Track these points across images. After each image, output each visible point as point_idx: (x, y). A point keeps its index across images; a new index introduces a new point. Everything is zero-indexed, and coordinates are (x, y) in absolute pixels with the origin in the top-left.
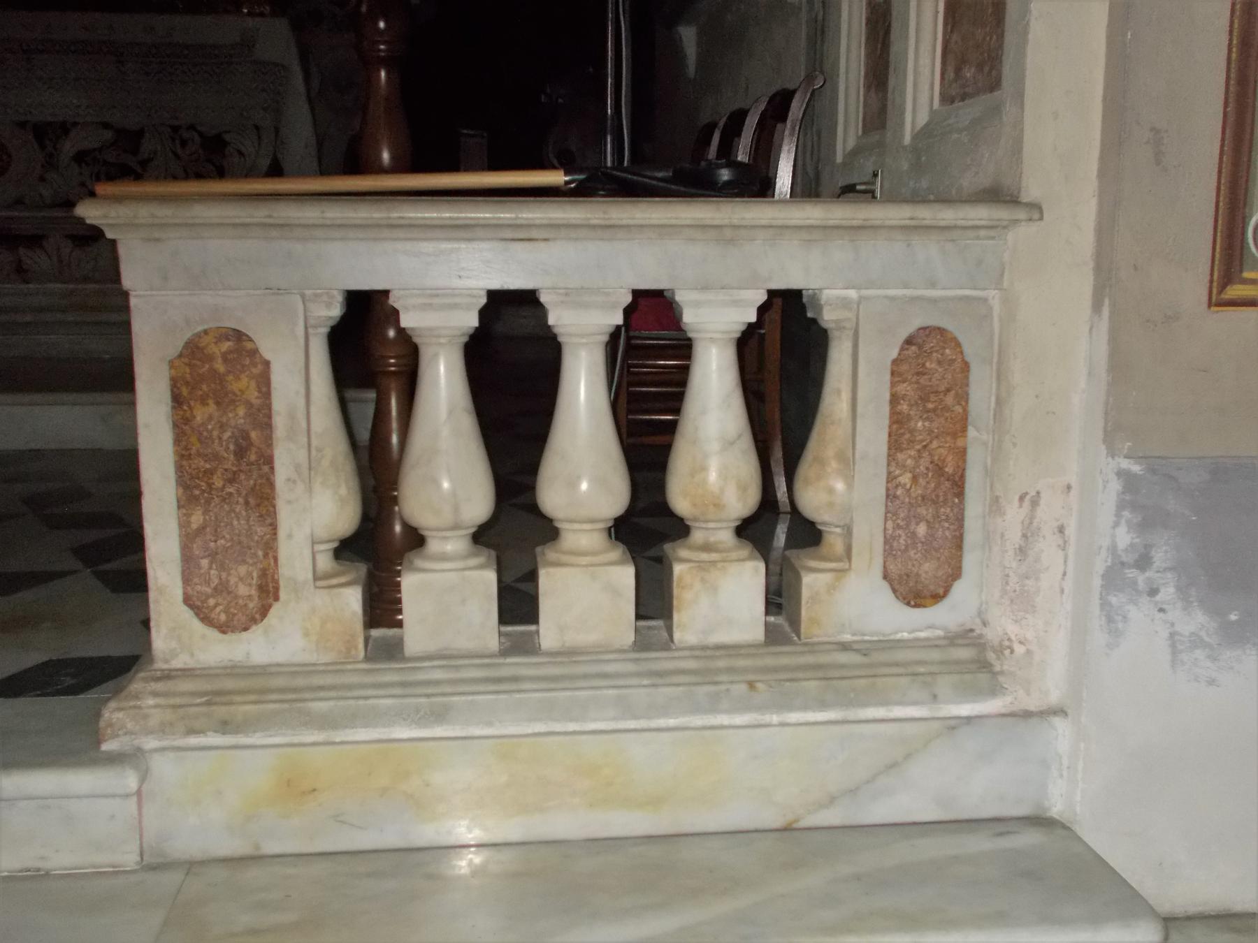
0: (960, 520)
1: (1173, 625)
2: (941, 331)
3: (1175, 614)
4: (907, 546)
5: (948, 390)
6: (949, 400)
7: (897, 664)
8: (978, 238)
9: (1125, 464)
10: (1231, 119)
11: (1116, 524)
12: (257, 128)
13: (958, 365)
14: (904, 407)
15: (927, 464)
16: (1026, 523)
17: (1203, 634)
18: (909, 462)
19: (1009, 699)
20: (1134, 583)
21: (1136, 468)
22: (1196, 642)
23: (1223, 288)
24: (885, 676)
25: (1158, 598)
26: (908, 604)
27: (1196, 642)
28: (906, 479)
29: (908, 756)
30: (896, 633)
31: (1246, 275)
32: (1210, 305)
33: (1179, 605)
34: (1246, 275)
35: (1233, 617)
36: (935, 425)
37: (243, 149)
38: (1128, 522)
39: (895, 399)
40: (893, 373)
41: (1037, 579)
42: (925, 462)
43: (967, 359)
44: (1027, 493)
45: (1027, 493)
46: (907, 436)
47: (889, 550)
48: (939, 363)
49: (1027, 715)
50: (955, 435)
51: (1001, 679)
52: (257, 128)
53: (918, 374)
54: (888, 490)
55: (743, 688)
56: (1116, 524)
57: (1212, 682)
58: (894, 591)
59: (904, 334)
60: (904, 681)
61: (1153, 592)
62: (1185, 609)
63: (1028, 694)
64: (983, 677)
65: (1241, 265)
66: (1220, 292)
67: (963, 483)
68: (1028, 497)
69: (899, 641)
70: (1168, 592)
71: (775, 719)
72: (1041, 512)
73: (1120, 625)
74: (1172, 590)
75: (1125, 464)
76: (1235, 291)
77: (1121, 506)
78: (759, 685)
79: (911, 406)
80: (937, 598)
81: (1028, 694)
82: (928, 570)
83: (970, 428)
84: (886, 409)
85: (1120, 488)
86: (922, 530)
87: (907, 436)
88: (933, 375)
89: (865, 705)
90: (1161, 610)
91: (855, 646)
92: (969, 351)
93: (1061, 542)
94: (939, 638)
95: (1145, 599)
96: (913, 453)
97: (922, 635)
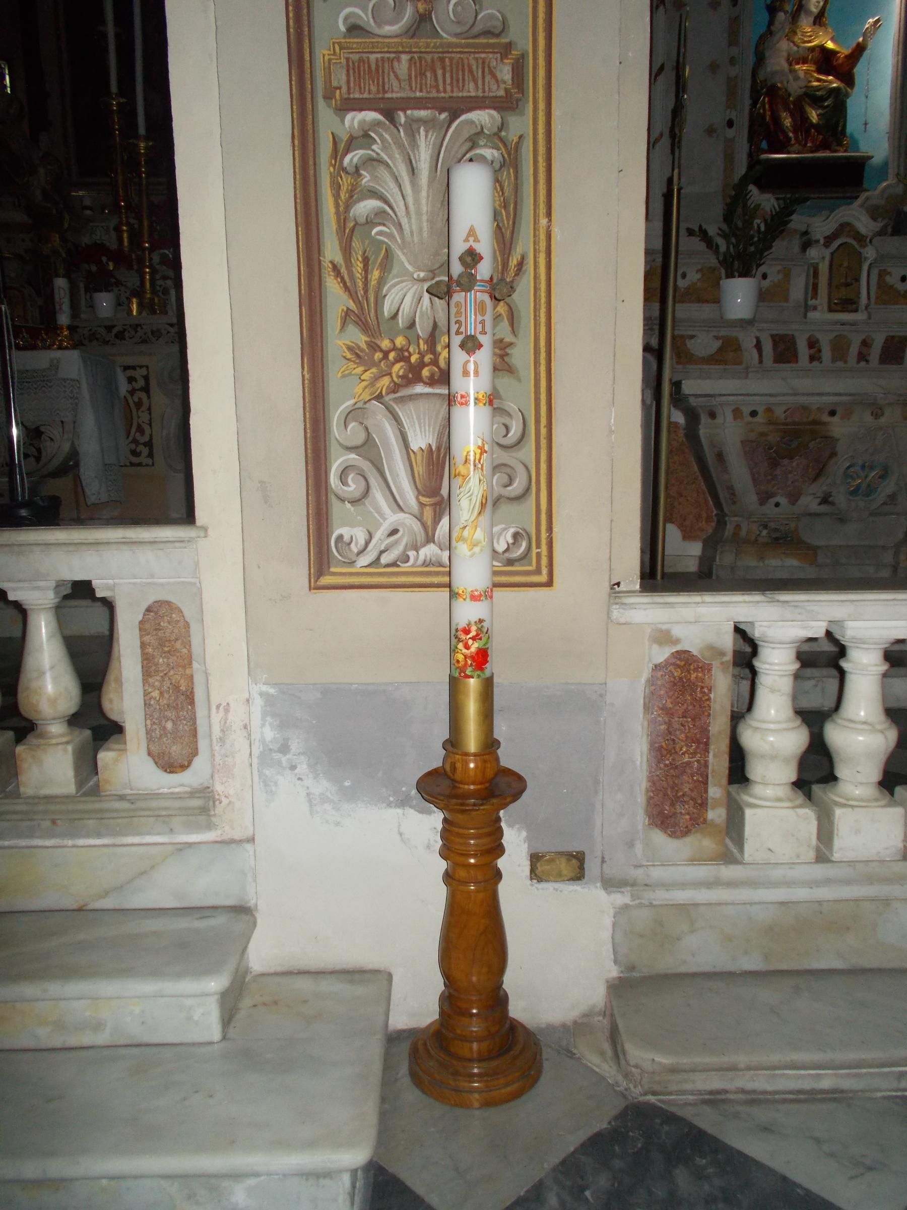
0: (194, 720)
1: (308, 788)
2: (168, 603)
3: (309, 781)
4: (161, 735)
5: (177, 640)
6: (178, 645)
7: (149, 809)
8: (176, 548)
9: (264, 688)
10: (311, 474)
11: (263, 726)
12: (62, 422)
13: (181, 624)
14: (150, 650)
15: (168, 685)
16: (223, 723)
17: (328, 794)
18: (157, 683)
19: (219, 832)
20: (279, 762)
21: (272, 691)
22: (324, 799)
23: (318, 578)
24: (109, 818)
25: (296, 771)
26: (166, 771)
27: (324, 799)
28: (156, 694)
29: (153, 867)
30: (159, 789)
31: (332, 570)
32: (310, 589)
33: (311, 776)
34: (332, 570)
35: (347, 784)
36: (171, 660)
37: (52, 436)
38: (270, 724)
39: (143, 645)
40: (140, 630)
41: (234, 757)
42: (167, 684)
43: (187, 620)
44: (220, 705)
45: (220, 705)
46: (154, 668)
47: (150, 739)
48: (169, 623)
49: (232, 842)
50: (184, 667)
51: (213, 819)
52: (62, 422)
53: (156, 630)
54: (145, 701)
55: (48, 823)
56: (263, 726)
57: (338, 824)
58: (156, 763)
59: (145, 606)
60: (152, 820)
61: (293, 768)
62: (315, 778)
63: (233, 829)
64: (202, 819)
65: (329, 563)
66: (316, 581)
67: (193, 697)
68: (221, 707)
69: (161, 794)
70: (303, 768)
71: (70, 843)
72: (231, 717)
73: (274, 788)
74: (305, 766)
75: (264, 688)
76: (326, 580)
77: (264, 716)
78: (59, 822)
79: (154, 649)
80: (184, 767)
81: (233, 829)
82: (176, 751)
83: (194, 662)
84: (139, 651)
85: (263, 703)
86: (169, 725)
87: (154, 668)
88: (168, 631)
89: (126, 835)
90: (299, 779)
91: (128, 798)
92: (187, 614)
93: (246, 734)
94: (186, 792)
95: (288, 772)
96: (158, 678)
97: (177, 790)
